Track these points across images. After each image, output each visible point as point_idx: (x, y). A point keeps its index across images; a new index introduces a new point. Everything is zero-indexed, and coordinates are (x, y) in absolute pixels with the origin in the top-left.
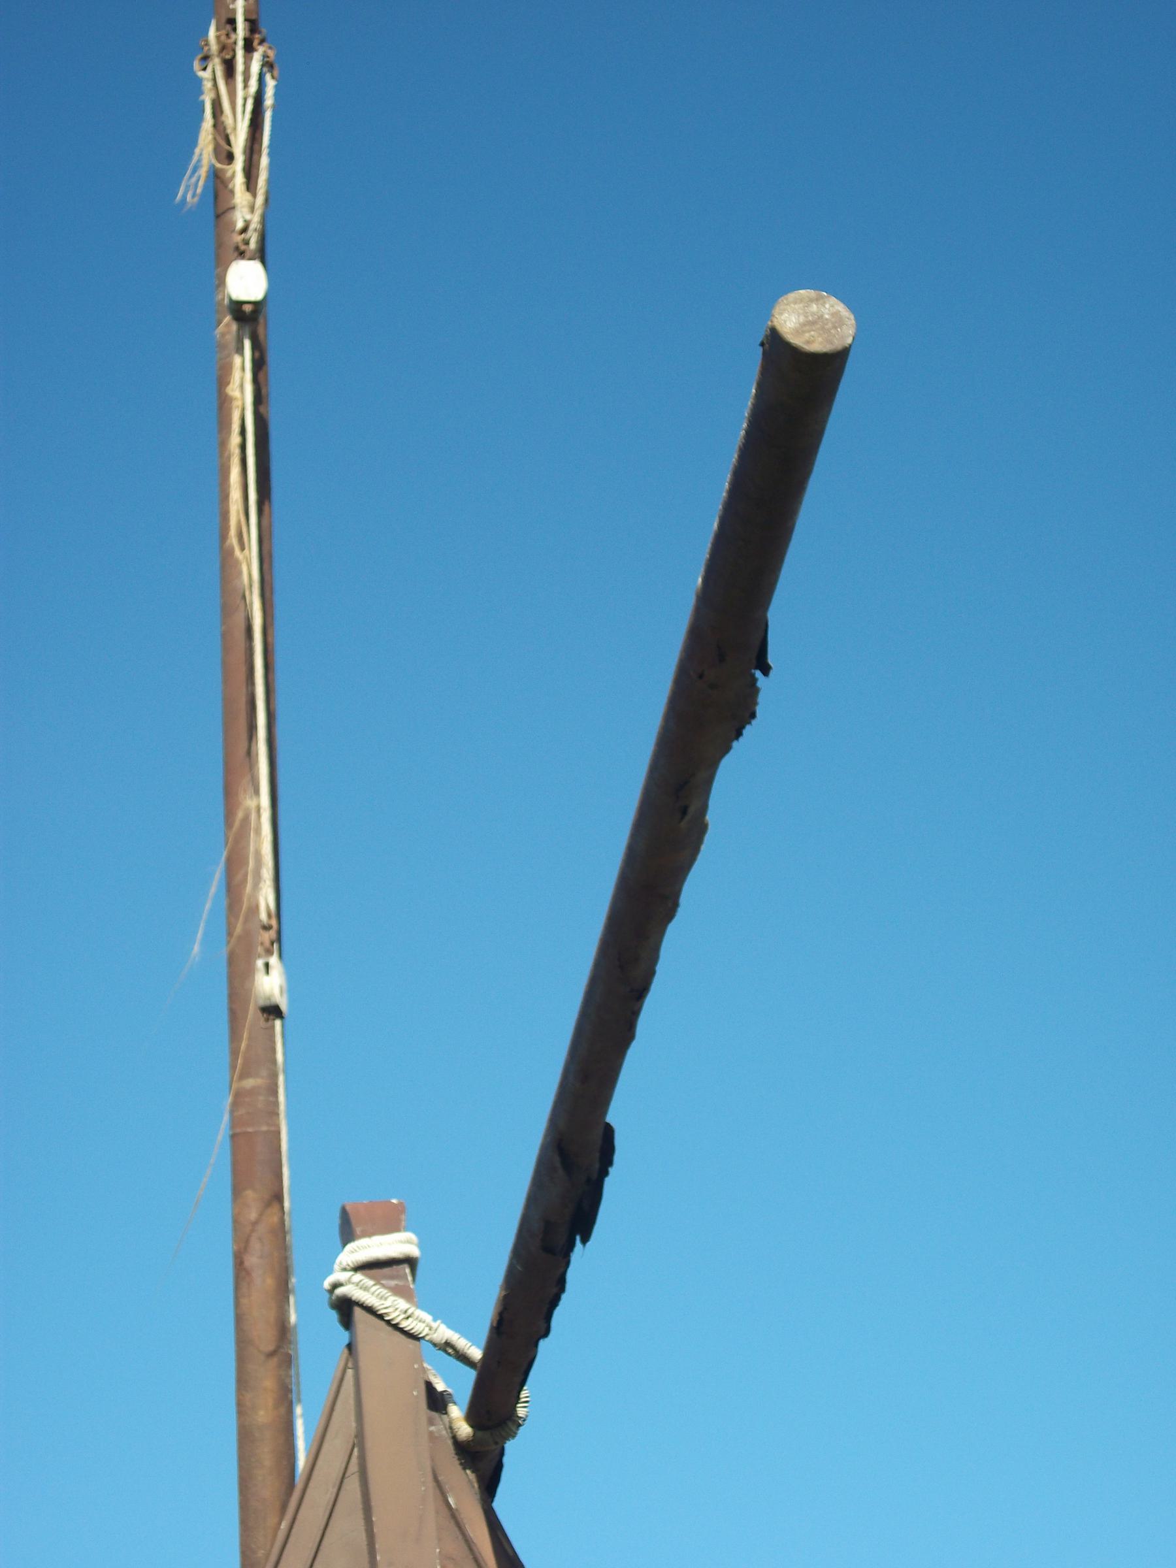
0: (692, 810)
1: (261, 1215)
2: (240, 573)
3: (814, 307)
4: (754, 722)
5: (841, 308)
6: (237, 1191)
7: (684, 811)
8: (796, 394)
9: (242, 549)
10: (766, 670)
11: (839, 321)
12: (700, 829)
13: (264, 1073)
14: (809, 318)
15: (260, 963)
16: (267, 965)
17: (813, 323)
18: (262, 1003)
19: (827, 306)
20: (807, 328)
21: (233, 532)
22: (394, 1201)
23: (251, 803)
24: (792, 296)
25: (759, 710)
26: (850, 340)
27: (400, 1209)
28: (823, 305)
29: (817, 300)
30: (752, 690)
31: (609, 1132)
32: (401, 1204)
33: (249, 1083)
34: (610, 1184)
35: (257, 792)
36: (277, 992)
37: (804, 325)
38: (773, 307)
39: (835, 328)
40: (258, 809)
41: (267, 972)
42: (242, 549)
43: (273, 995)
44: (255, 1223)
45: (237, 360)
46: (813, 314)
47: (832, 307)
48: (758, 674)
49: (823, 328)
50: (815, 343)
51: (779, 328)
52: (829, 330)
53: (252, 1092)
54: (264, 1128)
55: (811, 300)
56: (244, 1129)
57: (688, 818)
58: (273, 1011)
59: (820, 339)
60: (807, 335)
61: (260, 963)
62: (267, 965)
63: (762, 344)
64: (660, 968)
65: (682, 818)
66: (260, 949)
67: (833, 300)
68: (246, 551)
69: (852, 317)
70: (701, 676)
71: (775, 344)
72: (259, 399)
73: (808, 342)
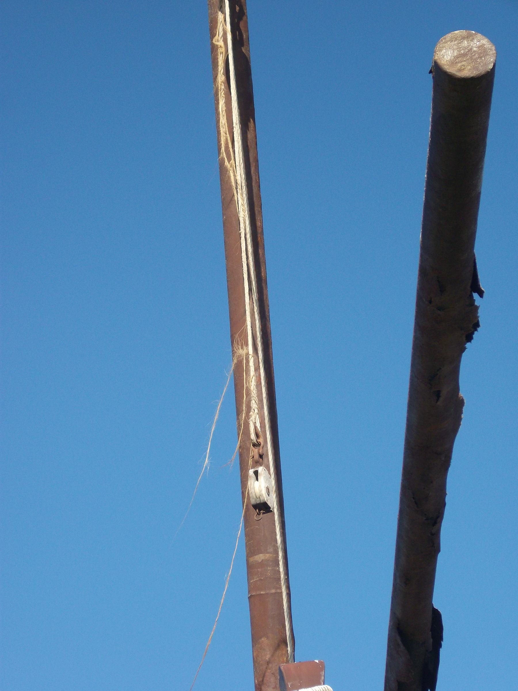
0: (444, 393)
1: (272, 656)
2: (229, 177)
3: (465, 43)
4: (479, 329)
5: (485, 42)
6: (255, 639)
7: (438, 394)
8: (461, 109)
9: (229, 160)
10: (481, 294)
11: (483, 52)
12: (459, 404)
13: (271, 550)
14: (461, 52)
15: (251, 472)
16: (256, 473)
17: (464, 55)
18: (253, 502)
19: (475, 41)
20: (460, 59)
21: (223, 149)
22: (317, 661)
23: (242, 352)
24: (449, 36)
25: (487, 307)
26: (491, 66)
27: (321, 667)
28: (472, 40)
29: (467, 37)
30: (472, 309)
31: (437, 616)
32: (321, 663)
33: (260, 557)
34: (442, 652)
35: (247, 345)
36: (264, 492)
37: (457, 57)
38: (435, 45)
39: (481, 58)
40: (247, 354)
41: (257, 479)
42: (229, 160)
43: (261, 495)
44: (268, 663)
45: (220, 16)
46: (465, 48)
47: (480, 42)
48: (476, 296)
49: (471, 58)
50: (467, 71)
51: (438, 61)
52: (476, 59)
53: (262, 564)
54: (273, 591)
55: (463, 38)
56: (258, 593)
57: (441, 399)
58: (263, 507)
59: (469, 67)
60: (459, 65)
61: (251, 472)
62: (256, 473)
63: (431, 72)
64: (448, 499)
65: (438, 400)
66: (250, 462)
67: (479, 36)
68: (232, 161)
69: (494, 48)
70: (430, 302)
71: (438, 72)
72: (239, 41)
73: (460, 70)
